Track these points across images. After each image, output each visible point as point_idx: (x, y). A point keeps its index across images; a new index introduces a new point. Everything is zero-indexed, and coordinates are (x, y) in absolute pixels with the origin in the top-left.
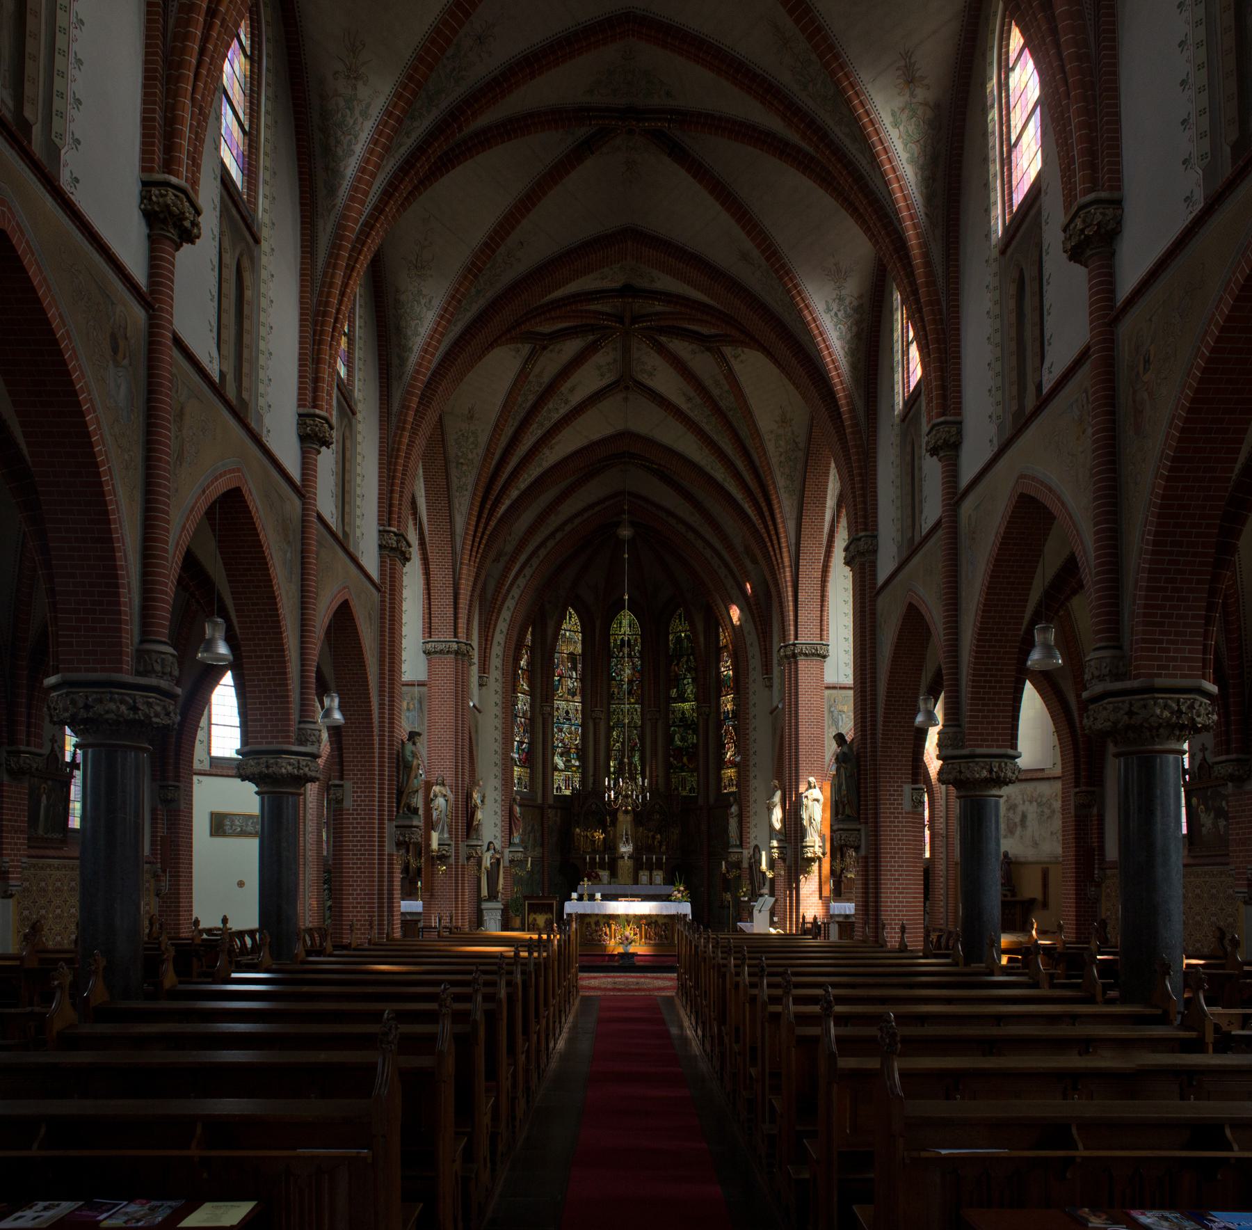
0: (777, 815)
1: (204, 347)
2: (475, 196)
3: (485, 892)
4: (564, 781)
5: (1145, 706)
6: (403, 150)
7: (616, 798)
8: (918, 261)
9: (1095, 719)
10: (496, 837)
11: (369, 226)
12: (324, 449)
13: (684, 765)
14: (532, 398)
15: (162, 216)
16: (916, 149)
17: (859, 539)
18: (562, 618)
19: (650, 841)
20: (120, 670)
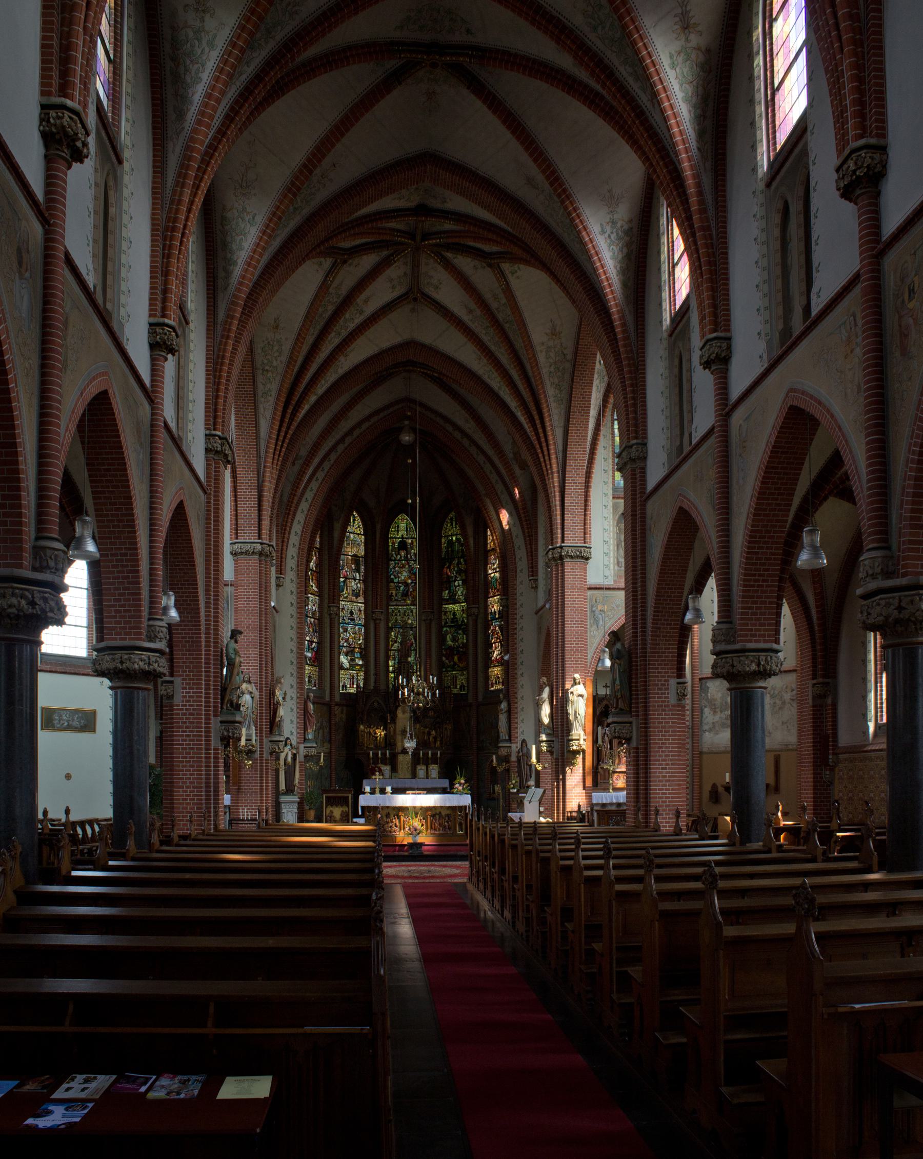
0: (546, 710)
1: (85, 262)
2: (297, 122)
3: (283, 786)
4: (350, 680)
5: (912, 602)
6: (244, 77)
7: (409, 695)
8: (692, 190)
9: (869, 614)
10: (292, 733)
11: (212, 148)
12: (170, 356)
13: (455, 664)
14: (331, 309)
15: (57, 137)
16: (690, 89)
17: (631, 447)
18: (347, 523)
20: (20, 566)
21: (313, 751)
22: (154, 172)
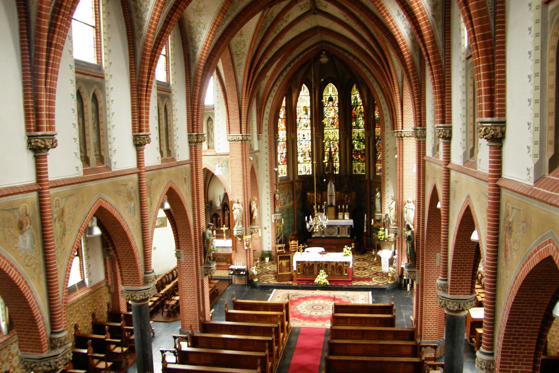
13: (359, 159)
19: (343, 198)
21: (278, 218)
22: (130, 58)
